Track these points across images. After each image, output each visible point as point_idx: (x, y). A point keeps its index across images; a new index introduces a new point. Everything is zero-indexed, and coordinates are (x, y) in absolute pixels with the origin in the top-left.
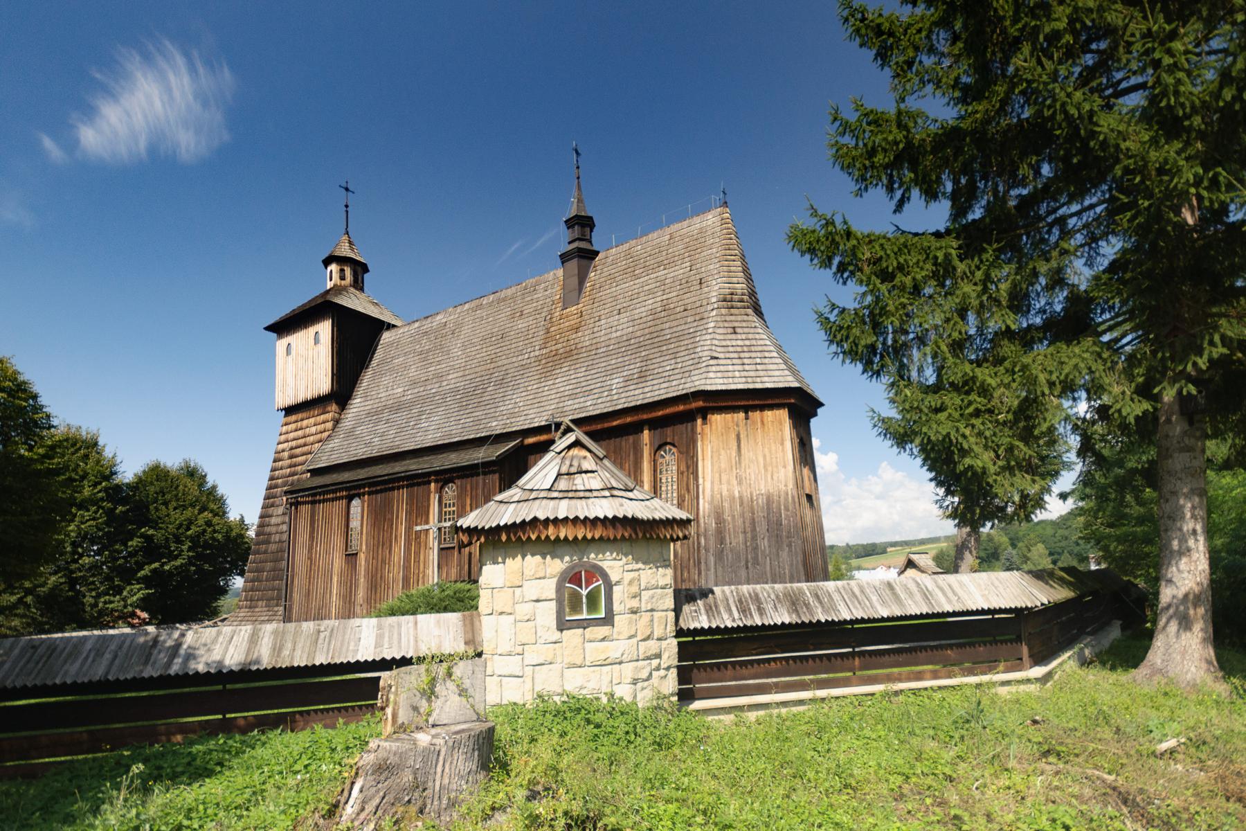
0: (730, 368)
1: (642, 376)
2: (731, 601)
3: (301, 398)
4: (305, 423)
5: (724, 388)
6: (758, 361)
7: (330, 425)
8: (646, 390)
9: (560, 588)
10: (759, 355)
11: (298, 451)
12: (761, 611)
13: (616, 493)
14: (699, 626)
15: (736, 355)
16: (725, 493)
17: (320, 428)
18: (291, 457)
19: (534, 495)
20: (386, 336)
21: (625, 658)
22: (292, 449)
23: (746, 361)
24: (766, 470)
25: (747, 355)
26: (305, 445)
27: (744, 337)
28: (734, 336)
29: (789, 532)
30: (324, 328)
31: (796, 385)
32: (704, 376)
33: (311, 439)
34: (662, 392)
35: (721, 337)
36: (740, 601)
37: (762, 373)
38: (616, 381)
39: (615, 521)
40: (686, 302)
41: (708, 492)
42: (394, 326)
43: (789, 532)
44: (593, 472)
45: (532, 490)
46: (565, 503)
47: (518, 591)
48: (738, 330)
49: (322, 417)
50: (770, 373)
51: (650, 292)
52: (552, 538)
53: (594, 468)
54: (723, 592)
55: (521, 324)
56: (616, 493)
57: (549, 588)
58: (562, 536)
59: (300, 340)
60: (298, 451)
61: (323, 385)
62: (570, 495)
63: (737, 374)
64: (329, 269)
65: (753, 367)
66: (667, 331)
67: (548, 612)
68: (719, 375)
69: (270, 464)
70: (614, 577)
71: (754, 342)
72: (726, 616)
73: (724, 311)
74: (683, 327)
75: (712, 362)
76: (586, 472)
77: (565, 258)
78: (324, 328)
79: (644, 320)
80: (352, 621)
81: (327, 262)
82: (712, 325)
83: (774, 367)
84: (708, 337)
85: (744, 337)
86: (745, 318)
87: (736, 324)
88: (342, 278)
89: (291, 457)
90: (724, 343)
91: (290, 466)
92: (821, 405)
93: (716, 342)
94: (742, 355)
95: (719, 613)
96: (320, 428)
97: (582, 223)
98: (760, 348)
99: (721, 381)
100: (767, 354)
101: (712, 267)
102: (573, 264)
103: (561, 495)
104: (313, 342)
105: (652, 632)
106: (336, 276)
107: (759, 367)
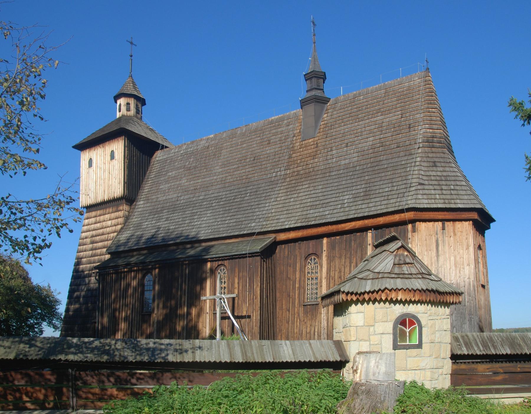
0: (433, 192)
1: (367, 195)
2: (478, 341)
3: (100, 199)
4: (102, 218)
6: (452, 187)
7: (121, 220)
8: (371, 205)
9: (395, 328)
10: (453, 183)
11: (98, 238)
12: (495, 347)
13: (425, 276)
14: (462, 353)
15: (436, 183)
17: (114, 222)
18: (92, 242)
19: (380, 276)
20: (159, 155)
21: (429, 367)
23: (444, 187)
24: (456, 266)
25: (444, 183)
26: (103, 234)
27: (441, 169)
28: (435, 169)
29: (470, 310)
30: (118, 147)
31: (481, 207)
32: (414, 197)
33: (108, 230)
34: (383, 207)
35: (426, 169)
36: (482, 340)
37: (455, 197)
38: (347, 198)
39: (422, 291)
40: (399, 141)
42: (166, 147)
43: (470, 310)
44: (412, 264)
45: (379, 273)
46: (399, 280)
47: (372, 329)
48: (438, 164)
49: (117, 214)
50: (461, 197)
51: (371, 132)
52: (394, 299)
53: (412, 262)
54: (473, 336)
55: (269, 150)
56: (425, 276)
57: (389, 327)
58: (399, 299)
59: (99, 154)
60: (98, 238)
61: (117, 189)
62: (401, 276)
63: (438, 196)
64: (119, 102)
65: (449, 192)
66: (385, 162)
67: (388, 341)
68: (425, 197)
69: (77, 247)
70: (423, 323)
71: (450, 174)
72: (476, 349)
73: (427, 149)
74: (396, 160)
75: (419, 187)
76: (408, 264)
77: (304, 103)
78: (118, 147)
79: (366, 152)
80: (276, 341)
81: (117, 98)
82: (418, 159)
83: (464, 193)
84: (416, 168)
85: (441, 169)
86: (442, 155)
87: (436, 160)
88: (128, 110)
89: (92, 242)
90: (428, 174)
91: (92, 249)
92: (493, 220)
93: (422, 173)
94: (441, 183)
95: (472, 347)
96: (114, 222)
97: (317, 77)
98: (453, 178)
99: (426, 201)
100: (458, 183)
101: (418, 116)
102: (311, 108)
103: (396, 276)
104: (109, 158)
105: (440, 354)
106: (124, 108)
107: (452, 192)
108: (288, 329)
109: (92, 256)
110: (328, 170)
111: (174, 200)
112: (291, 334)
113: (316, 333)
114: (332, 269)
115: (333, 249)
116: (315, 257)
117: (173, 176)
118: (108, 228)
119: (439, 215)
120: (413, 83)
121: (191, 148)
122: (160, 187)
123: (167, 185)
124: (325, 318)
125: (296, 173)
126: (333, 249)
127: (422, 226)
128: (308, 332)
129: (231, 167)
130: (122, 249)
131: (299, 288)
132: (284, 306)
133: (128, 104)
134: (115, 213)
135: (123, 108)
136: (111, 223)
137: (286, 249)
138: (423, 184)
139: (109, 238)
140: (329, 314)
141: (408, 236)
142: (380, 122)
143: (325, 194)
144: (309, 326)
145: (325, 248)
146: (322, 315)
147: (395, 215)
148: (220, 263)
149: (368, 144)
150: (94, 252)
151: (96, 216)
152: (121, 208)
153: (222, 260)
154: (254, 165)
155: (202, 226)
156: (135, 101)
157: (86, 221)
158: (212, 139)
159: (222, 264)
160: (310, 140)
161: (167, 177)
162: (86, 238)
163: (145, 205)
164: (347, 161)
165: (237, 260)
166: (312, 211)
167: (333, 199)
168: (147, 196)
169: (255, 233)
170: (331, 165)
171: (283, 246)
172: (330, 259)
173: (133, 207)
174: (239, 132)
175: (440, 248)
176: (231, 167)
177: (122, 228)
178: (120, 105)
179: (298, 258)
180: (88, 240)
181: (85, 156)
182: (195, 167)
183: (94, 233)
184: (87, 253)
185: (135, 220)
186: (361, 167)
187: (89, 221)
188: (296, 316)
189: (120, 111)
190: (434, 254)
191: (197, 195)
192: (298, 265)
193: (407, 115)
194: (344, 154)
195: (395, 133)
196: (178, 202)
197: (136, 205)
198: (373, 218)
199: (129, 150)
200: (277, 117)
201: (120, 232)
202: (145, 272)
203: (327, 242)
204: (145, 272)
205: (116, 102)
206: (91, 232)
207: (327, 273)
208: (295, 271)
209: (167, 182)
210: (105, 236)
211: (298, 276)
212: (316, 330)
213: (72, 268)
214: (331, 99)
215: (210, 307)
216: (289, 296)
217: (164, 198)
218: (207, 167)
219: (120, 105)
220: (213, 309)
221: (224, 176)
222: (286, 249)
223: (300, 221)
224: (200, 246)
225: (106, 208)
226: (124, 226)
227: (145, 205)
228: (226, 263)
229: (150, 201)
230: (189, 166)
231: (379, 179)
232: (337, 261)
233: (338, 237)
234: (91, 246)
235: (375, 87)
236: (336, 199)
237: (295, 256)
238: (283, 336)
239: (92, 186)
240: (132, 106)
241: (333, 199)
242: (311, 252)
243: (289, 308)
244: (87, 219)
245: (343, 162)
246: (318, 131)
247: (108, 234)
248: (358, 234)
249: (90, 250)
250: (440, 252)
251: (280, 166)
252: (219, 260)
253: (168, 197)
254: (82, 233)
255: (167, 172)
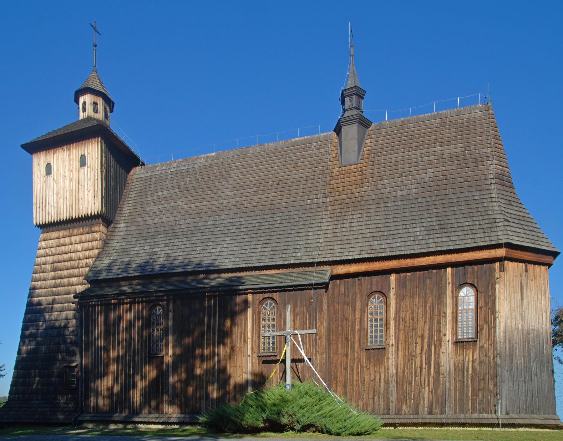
3: (65, 215)
5: (519, 243)
11: (63, 265)
16: (514, 326)
20: (137, 172)
22: (54, 262)
27: (516, 209)
30: (93, 151)
41: (502, 325)
49: (91, 236)
51: (429, 163)
59: (62, 160)
61: (91, 202)
78: (93, 151)
81: (80, 93)
88: (96, 111)
89: (55, 270)
91: (54, 278)
104: (78, 164)
106: (89, 108)
108: (345, 376)
109: (55, 286)
110: (382, 201)
111: (170, 224)
112: (350, 381)
113: (382, 381)
114: (402, 309)
115: (403, 287)
116: (380, 296)
117: (165, 196)
118: (78, 253)
119: (526, 255)
120: (474, 115)
121: (185, 166)
122: (148, 209)
123: (157, 207)
124: (394, 363)
125: (339, 202)
126: (403, 287)
127: (509, 265)
128: (482, 381)
129: (247, 191)
130: (103, 276)
131: (360, 330)
132: (340, 350)
133: (95, 104)
134: (88, 235)
135: (89, 108)
136: (83, 247)
137: (342, 285)
138: (508, 221)
139: (81, 265)
140: (399, 359)
141: (495, 276)
142: (440, 153)
143: (386, 225)
144: (372, 372)
145: (393, 285)
146: (391, 361)
147: (484, 251)
148: (266, 295)
149: (428, 175)
150: (58, 281)
151: (58, 238)
152: (97, 228)
153: (270, 292)
154: (279, 190)
155: (225, 254)
156: (104, 102)
157: (43, 244)
158: (214, 158)
159: (268, 298)
160: (352, 167)
161: (155, 198)
162: (45, 264)
163: (129, 229)
164: (404, 192)
165: (292, 293)
166: (376, 243)
167: (401, 231)
168: (130, 218)
169: (314, 263)
170: (384, 195)
171: (338, 281)
172: (400, 298)
173: (111, 230)
174: (251, 152)
175: (524, 291)
176: (247, 191)
177: (99, 254)
178: (84, 103)
179: (358, 296)
180: (48, 267)
181: (39, 161)
182: (195, 188)
183: (56, 258)
184: (48, 282)
185: (116, 244)
186: (424, 200)
187: (48, 243)
188: (356, 362)
189: (84, 110)
190: (518, 296)
191: (203, 219)
192: (358, 304)
193: (472, 148)
194: (399, 184)
195: (459, 167)
196: (178, 227)
197: (114, 228)
198: (457, 253)
199: (105, 157)
200: (303, 138)
201: (99, 256)
202: (152, 304)
203: (396, 279)
204: (152, 304)
205: (77, 101)
206: (52, 257)
207: (396, 314)
208: (354, 311)
209: (156, 203)
210: (74, 262)
211: (358, 316)
212: (382, 377)
213: (25, 301)
214: (373, 124)
215: (252, 348)
216: (347, 339)
217: (156, 221)
218: (213, 188)
219: (84, 103)
220: (257, 351)
221: (237, 200)
222: (342, 285)
223: (364, 252)
224: (219, 278)
225: (73, 228)
226: (103, 251)
227: (129, 229)
228: (275, 296)
229: (135, 224)
230: (186, 186)
231: (452, 213)
232: (408, 301)
233: (409, 274)
234: (52, 274)
235: (426, 115)
236: (404, 231)
237: (355, 294)
238: (339, 384)
239: (52, 199)
240: (100, 108)
241: (401, 231)
242: (374, 289)
243: (347, 352)
244: (44, 240)
245: (399, 193)
246: (360, 157)
247: (79, 260)
248: (434, 271)
249: (51, 279)
250: (525, 296)
251: (315, 192)
252: (265, 292)
253: (160, 221)
254: (37, 257)
255: (155, 191)
